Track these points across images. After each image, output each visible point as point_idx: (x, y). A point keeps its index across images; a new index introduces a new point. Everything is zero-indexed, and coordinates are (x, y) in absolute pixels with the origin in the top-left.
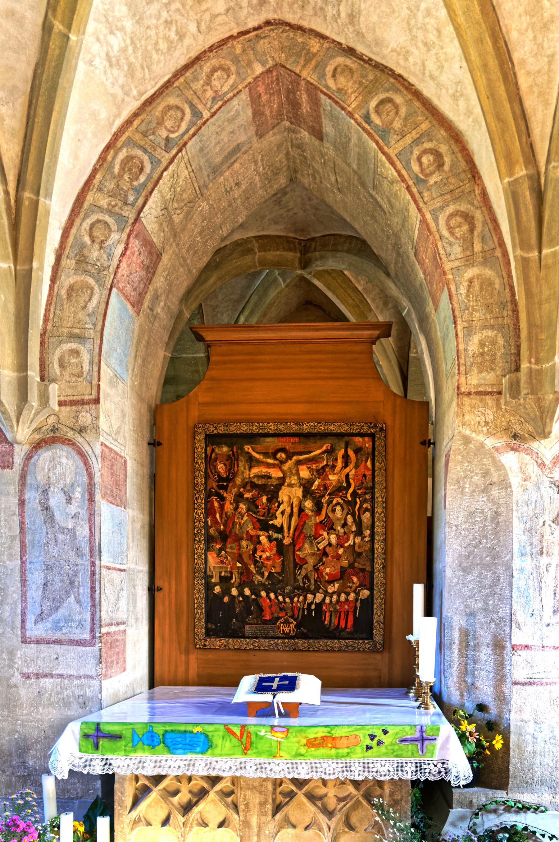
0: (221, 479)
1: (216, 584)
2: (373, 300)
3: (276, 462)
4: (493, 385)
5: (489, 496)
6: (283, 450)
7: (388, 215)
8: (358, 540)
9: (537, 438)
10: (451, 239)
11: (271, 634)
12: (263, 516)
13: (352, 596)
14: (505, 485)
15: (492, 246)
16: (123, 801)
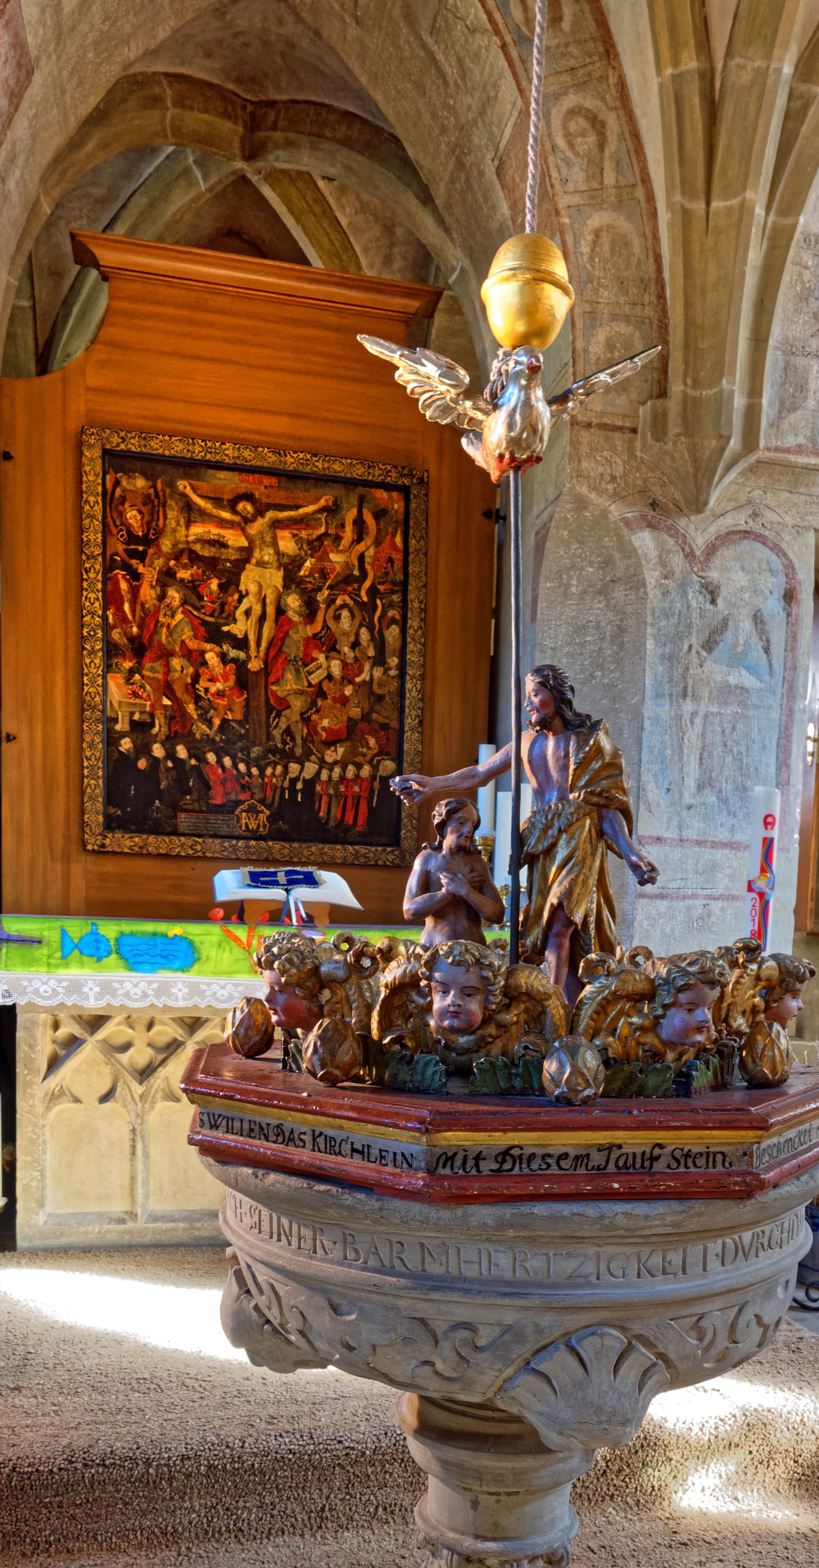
0: (132, 538)
1: (123, 735)
2: (366, 250)
3: (237, 518)
4: (625, 416)
5: (608, 601)
6: (248, 497)
7: (452, 89)
8: (378, 673)
9: (685, 510)
10: (569, 154)
11: (225, 830)
12: (211, 615)
13: (366, 771)
14: (636, 582)
15: (631, 181)
16: (32, 1060)
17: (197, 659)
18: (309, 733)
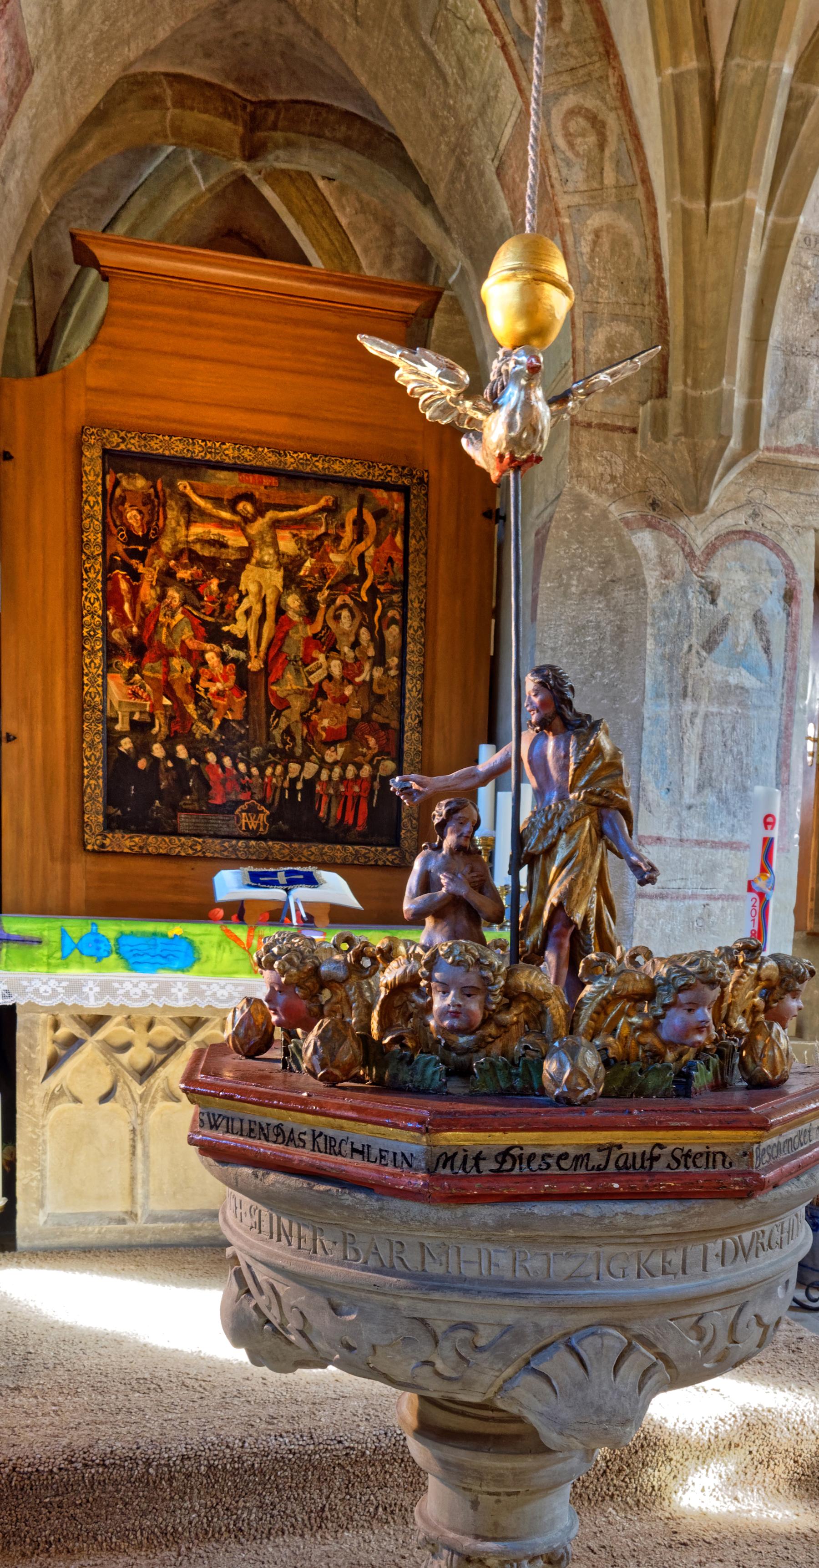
0: (132, 538)
1: (123, 735)
2: (366, 250)
3: (237, 518)
4: (625, 416)
5: (608, 601)
6: (248, 497)
7: (452, 89)
8: (378, 673)
9: (685, 510)
10: (569, 154)
11: (225, 830)
12: (211, 615)
13: (366, 771)
14: (636, 582)
15: (631, 181)
16: (32, 1060)
17: (197, 659)
18: (309, 733)
